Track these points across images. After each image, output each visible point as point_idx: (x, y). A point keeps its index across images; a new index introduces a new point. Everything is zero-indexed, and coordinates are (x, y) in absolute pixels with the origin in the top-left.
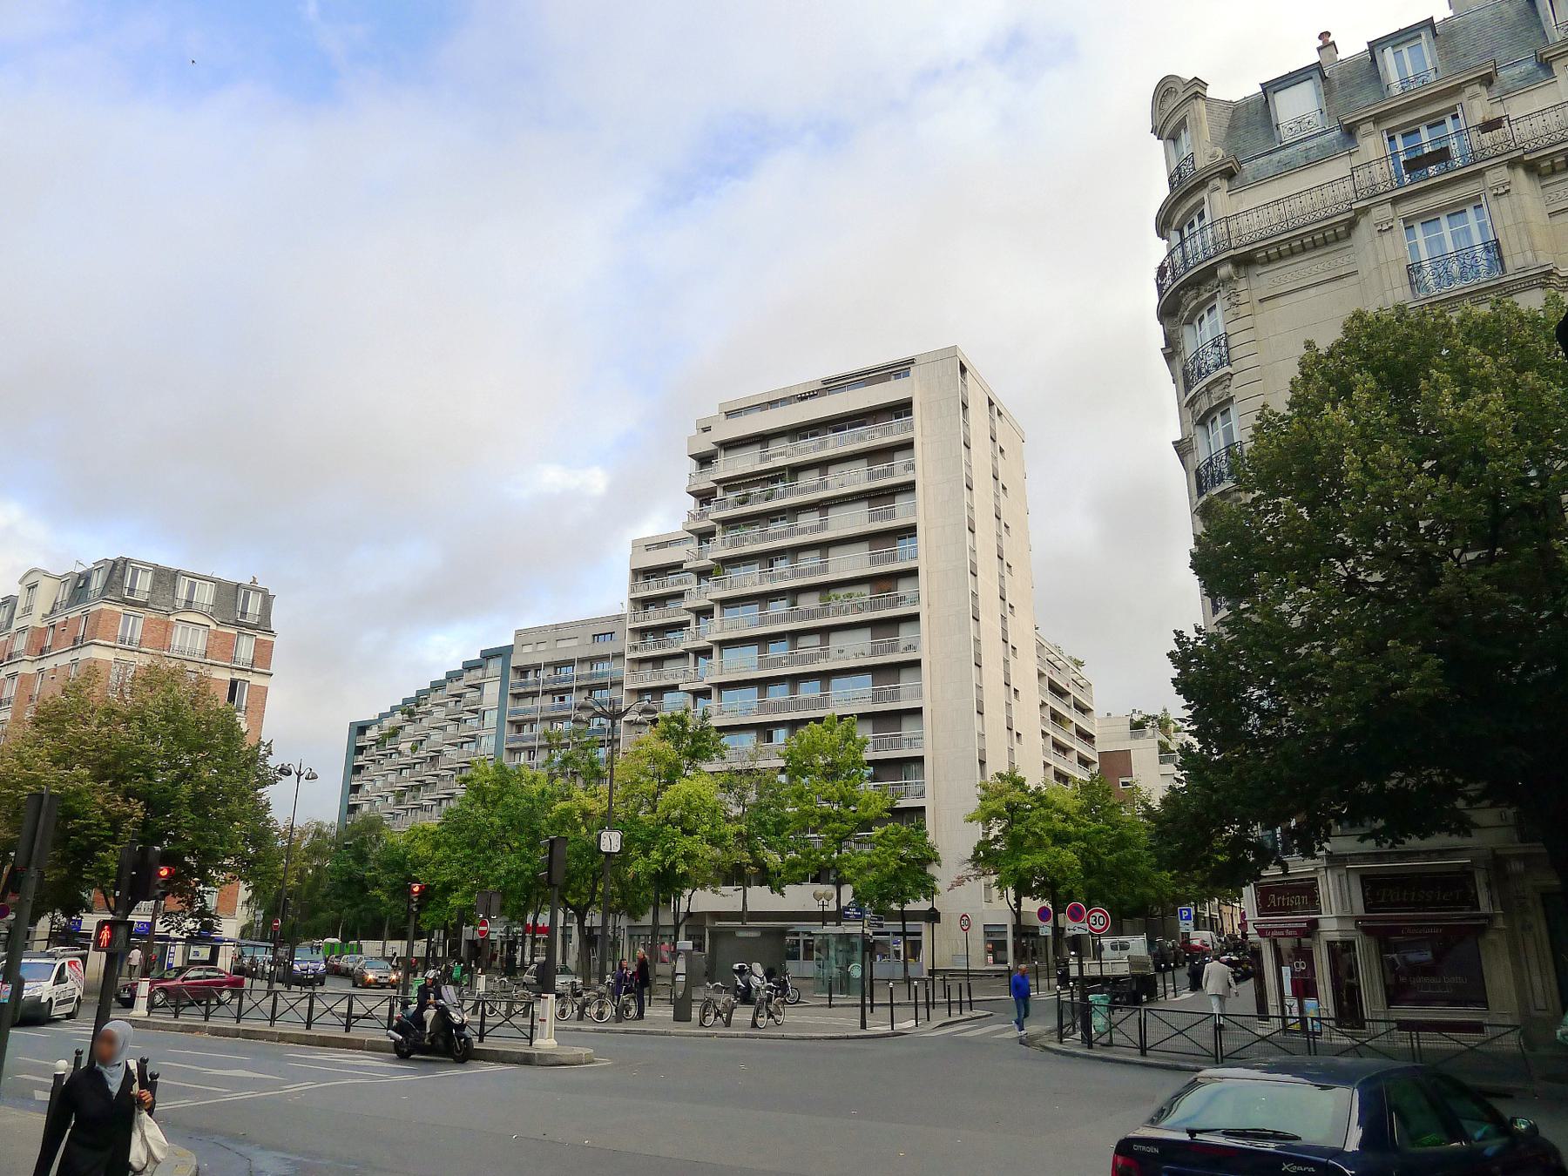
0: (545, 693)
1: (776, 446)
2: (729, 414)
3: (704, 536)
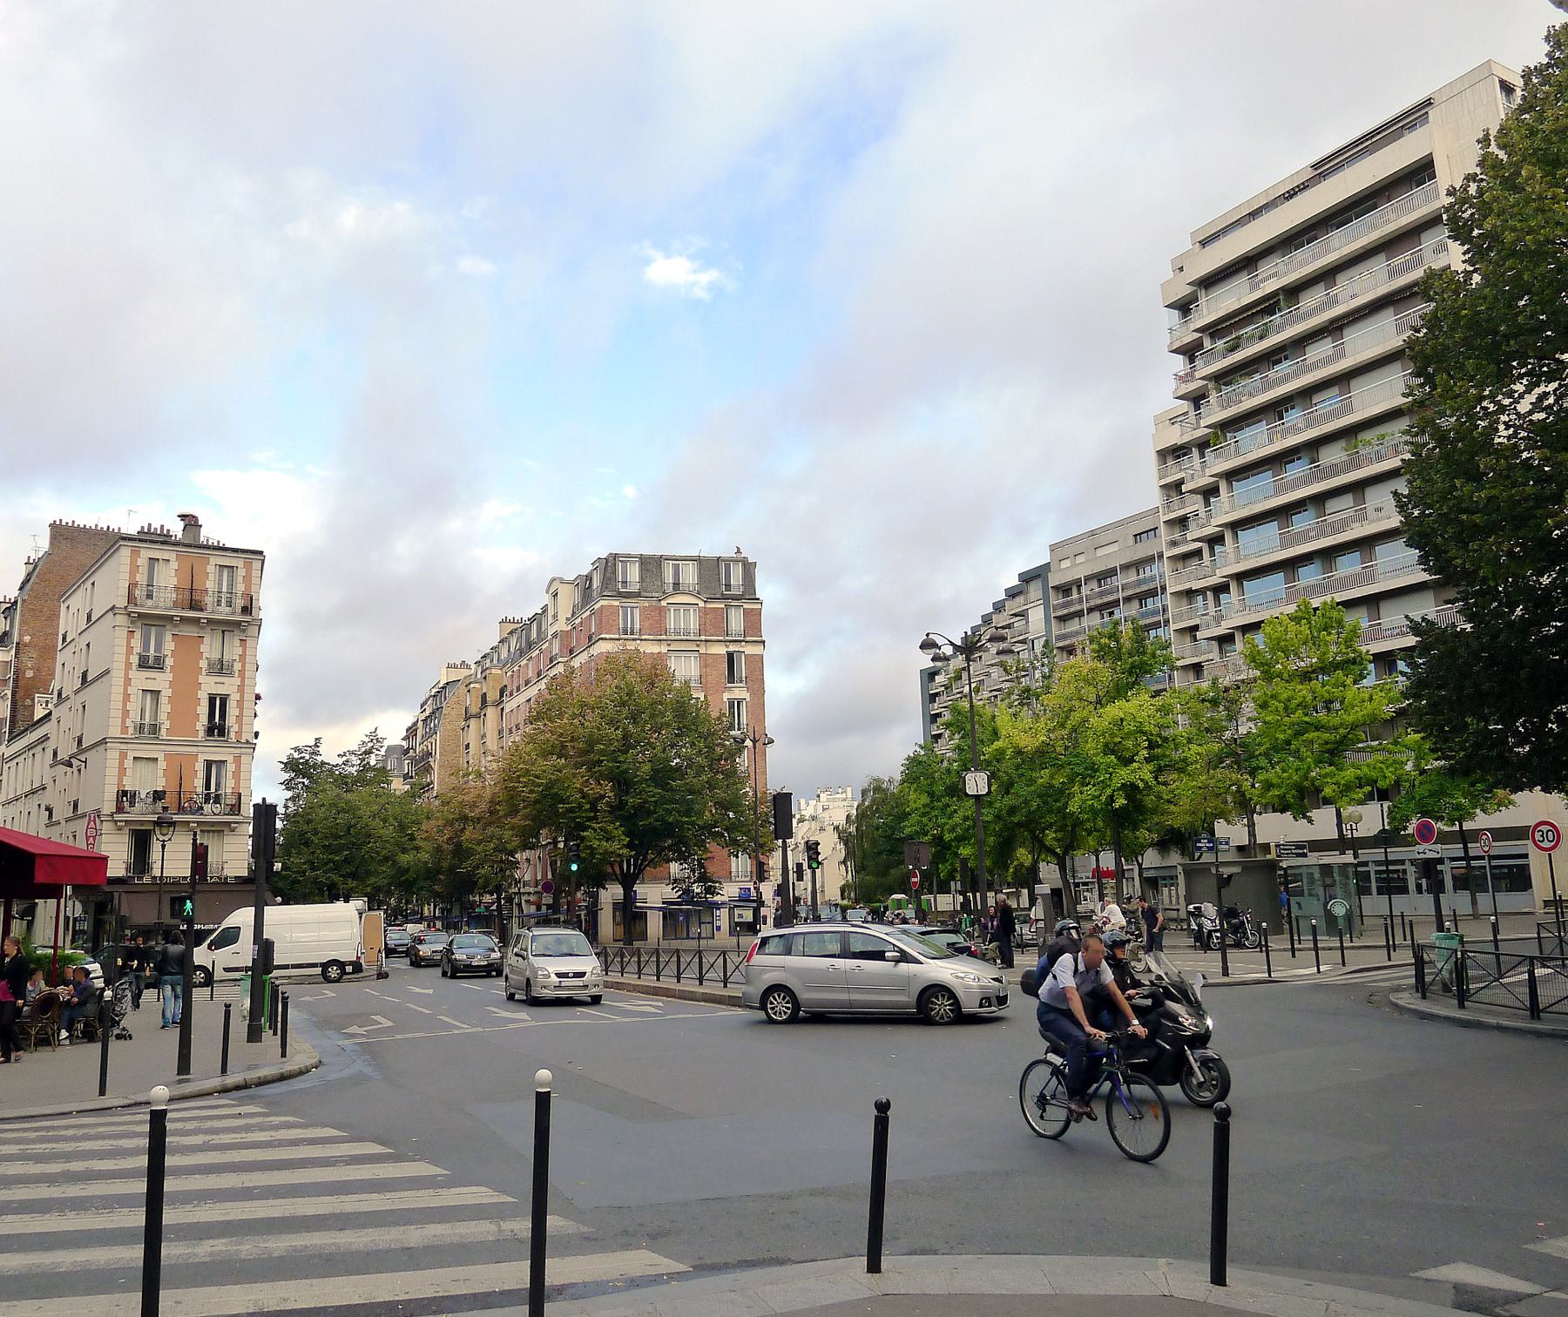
0: (1090, 610)
1: (1265, 268)
2: (1204, 243)
3: (1197, 399)
